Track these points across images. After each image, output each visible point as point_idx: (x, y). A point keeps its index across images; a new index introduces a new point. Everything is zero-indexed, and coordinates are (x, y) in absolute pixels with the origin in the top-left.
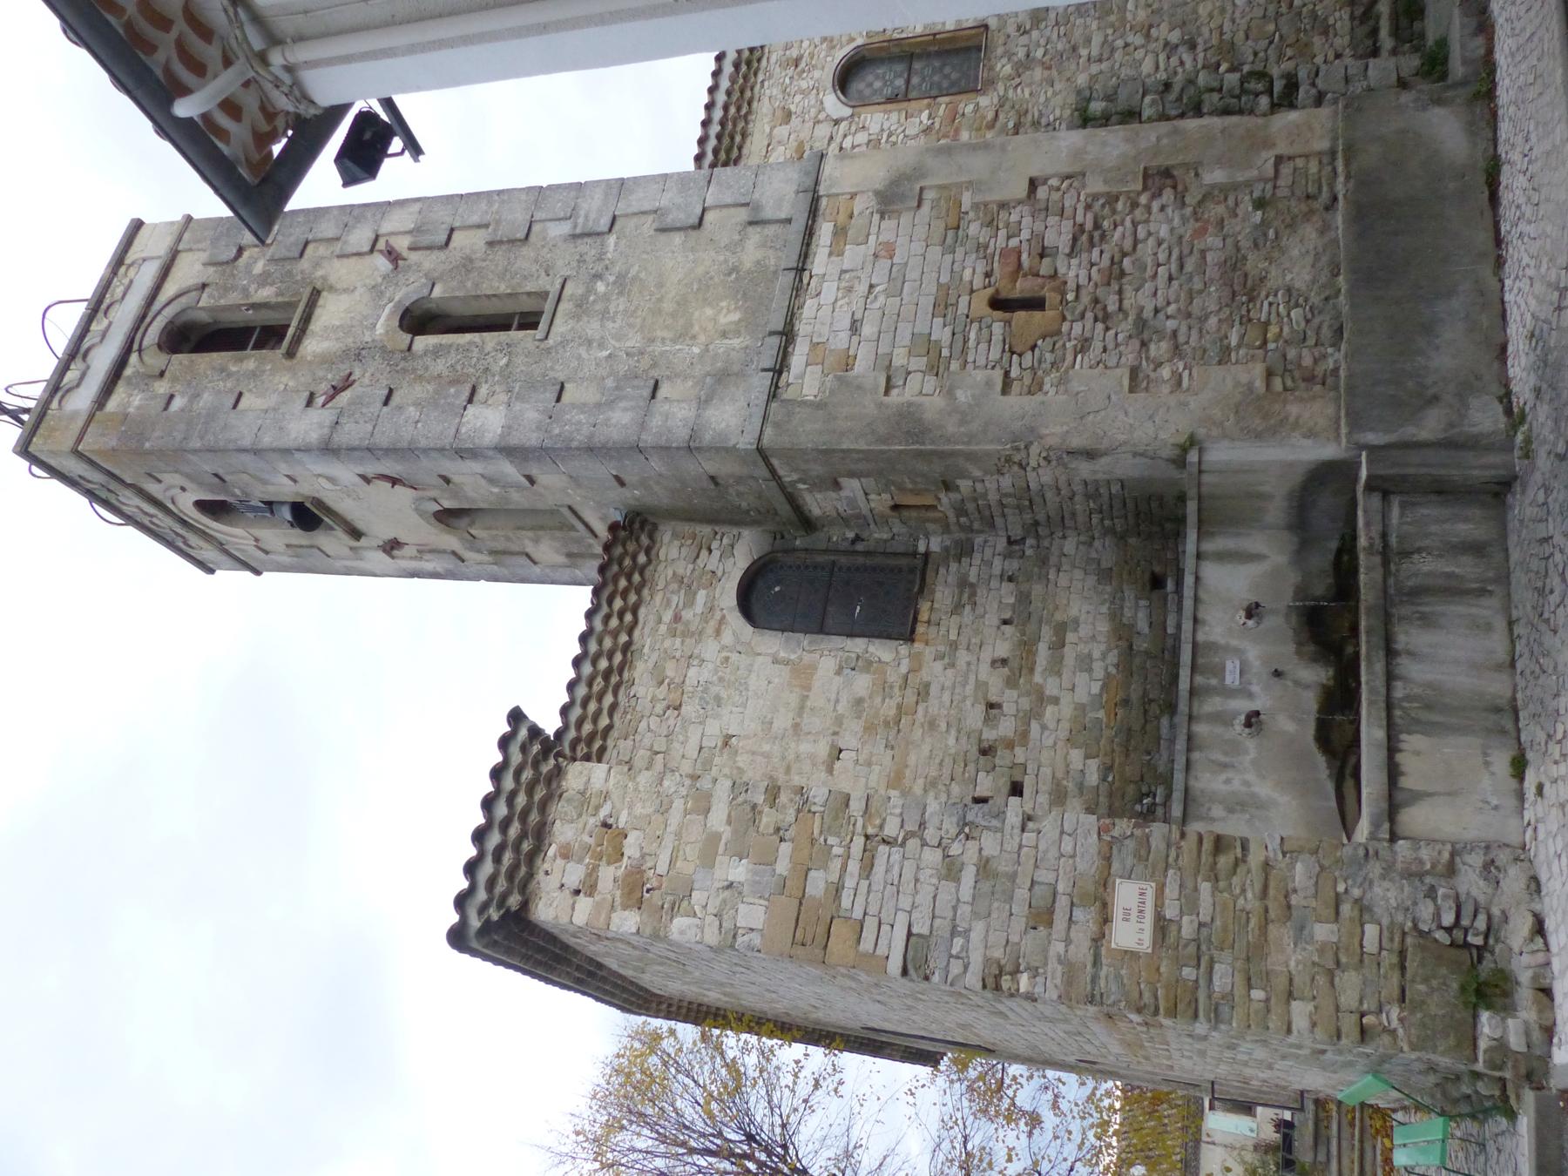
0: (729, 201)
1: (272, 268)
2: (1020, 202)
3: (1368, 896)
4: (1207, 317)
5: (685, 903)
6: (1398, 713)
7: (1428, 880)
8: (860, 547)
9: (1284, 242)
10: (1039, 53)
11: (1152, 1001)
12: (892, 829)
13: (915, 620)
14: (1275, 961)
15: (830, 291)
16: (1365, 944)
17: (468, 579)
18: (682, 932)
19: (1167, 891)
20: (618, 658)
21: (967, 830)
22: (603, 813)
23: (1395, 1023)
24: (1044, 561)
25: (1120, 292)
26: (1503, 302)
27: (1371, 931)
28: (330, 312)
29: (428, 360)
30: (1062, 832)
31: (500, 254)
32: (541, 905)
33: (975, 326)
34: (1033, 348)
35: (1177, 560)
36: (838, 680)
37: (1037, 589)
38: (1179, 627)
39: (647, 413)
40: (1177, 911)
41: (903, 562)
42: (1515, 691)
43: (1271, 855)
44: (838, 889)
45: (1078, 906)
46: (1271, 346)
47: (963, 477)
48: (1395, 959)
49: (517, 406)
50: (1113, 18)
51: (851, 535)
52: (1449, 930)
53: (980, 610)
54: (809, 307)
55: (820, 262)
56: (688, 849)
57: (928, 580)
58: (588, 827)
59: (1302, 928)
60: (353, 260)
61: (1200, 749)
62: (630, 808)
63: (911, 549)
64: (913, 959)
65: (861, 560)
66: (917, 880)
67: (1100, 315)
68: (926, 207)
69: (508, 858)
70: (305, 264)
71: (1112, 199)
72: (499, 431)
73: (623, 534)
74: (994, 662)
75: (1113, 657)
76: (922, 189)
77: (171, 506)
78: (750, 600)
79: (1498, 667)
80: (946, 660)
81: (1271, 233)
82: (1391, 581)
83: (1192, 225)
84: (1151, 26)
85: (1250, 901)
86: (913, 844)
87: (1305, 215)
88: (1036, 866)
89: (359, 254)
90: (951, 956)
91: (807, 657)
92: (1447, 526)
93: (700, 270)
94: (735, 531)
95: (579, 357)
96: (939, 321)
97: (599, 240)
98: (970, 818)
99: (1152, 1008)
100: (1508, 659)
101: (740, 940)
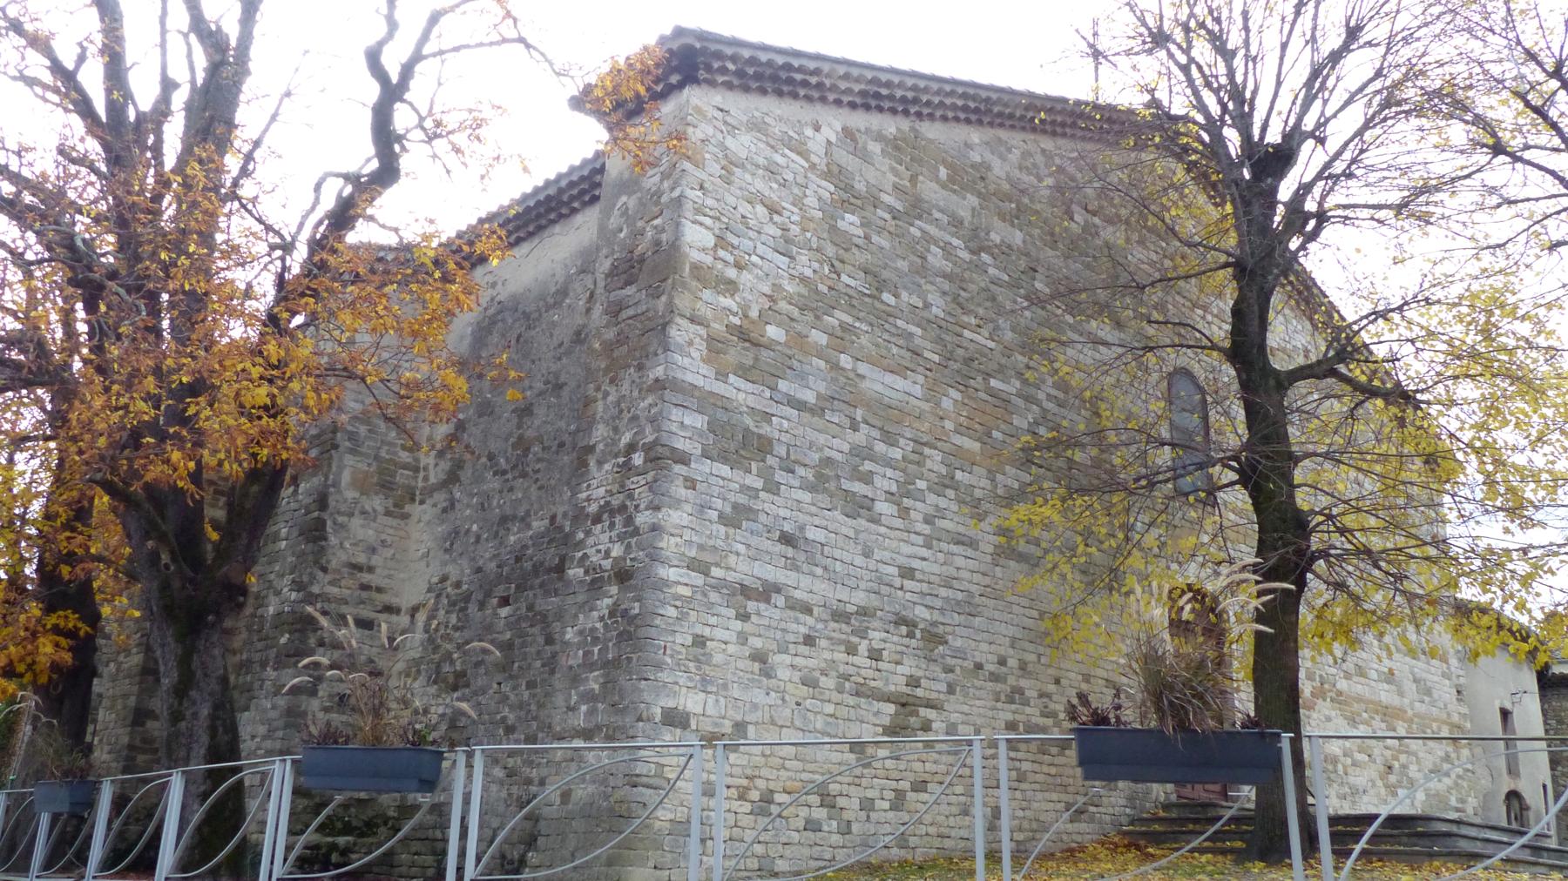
30: (784, 759)
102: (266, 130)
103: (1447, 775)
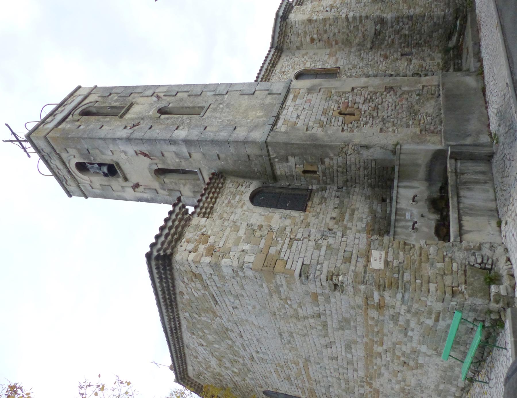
0: (263, 89)
1: (119, 98)
2: (349, 92)
3: (453, 256)
4: (402, 118)
5: (227, 255)
6: (461, 211)
7: (473, 251)
8: (290, 187)
9: (425, 103)
10: (354, 74)
11: (383, 283)
12: (299, 236)
13: (307, 206)
14: (424, 272)
15: (291, 109)
16: (453, 268)
17: (158, 202)
18: (225, 263)
19: (389, 254)
20: (208, 210)
21: (324, 237)
22: (202, 231)
23: (463, 289)
24: (349, 193)
25: (377, 112)
26: (488, 115)
27: (455, 265)
28: (135, 109)
29: (165, 120)
30: (355, 238)
31: (191, 98)
32: (177, 255)
33: (334, 118)
34: (351, 123)
35: (390, 194)
36: (280, 221)
37: (346, 200)
38: (391, 211)
39: (232, 133)
40: (392, 259)
41: (304, 193)
42: (497, 206)
43: (422, 245)
44: (280, 252)
45: (360, 257)
46: (421, 125)
47: (328, 157)
48: (463, 272)
49: (191, 131)
50: (375, 68)
51: (288, 184)
52: (480, 264)
53: (327, 204)
54: (285, 112)
55: (289, 102)
56: (230, 241)
57: (312, 196)
58: (197, 234)
59: (432, 264)
60: (145, 98)
61: (398, 235)
62: (212, 229)
63: (307, 188)
64: (304, 271)
65: (290, 191)
66: (306, 250)
67: (371, 117)
68: (321, 93)
69: (169, 238)
70: (130, 98)
71: (376, 93)
72: (185, 136)
73: (215, 177)
74: (331, 218)
75: (369, 218)
76: (320, 88)
77: (67, 164)
78: (255, 199)
79: (492, 201)
80: (316, 217)
81: (421, 101)
82: (458, 180)
83: (398, 99)
84: (386, 71)
85: (416, 257)
86: (306, 240)
87: (431, 98)
88: (346, 246)
89: (148, 96)
90: (317, 270)
91: (270, 214)
92: (474, 168)
93: (252, 104)
94: (251, 181)
95: (212, 121)
96: (323, 116)
97: (222, 96)
98: (325, 234)
99: (383, 286)
100: (494, 199)
101: (245, 265)
102: (11, 129)
103: (408, 321)
